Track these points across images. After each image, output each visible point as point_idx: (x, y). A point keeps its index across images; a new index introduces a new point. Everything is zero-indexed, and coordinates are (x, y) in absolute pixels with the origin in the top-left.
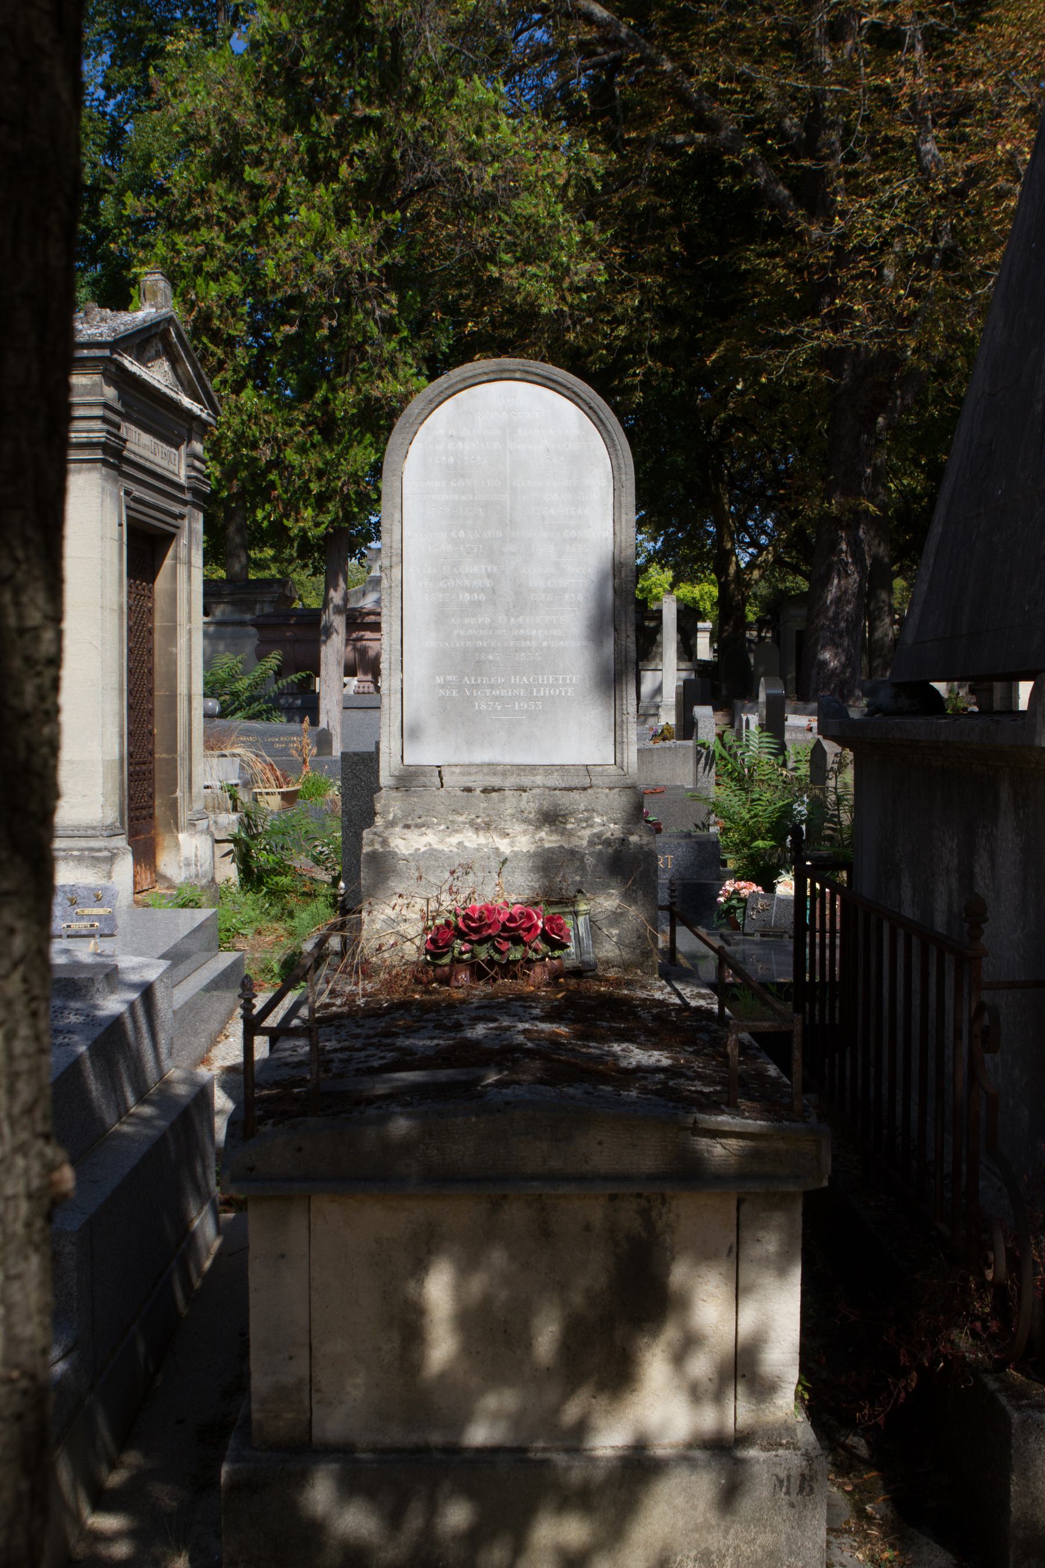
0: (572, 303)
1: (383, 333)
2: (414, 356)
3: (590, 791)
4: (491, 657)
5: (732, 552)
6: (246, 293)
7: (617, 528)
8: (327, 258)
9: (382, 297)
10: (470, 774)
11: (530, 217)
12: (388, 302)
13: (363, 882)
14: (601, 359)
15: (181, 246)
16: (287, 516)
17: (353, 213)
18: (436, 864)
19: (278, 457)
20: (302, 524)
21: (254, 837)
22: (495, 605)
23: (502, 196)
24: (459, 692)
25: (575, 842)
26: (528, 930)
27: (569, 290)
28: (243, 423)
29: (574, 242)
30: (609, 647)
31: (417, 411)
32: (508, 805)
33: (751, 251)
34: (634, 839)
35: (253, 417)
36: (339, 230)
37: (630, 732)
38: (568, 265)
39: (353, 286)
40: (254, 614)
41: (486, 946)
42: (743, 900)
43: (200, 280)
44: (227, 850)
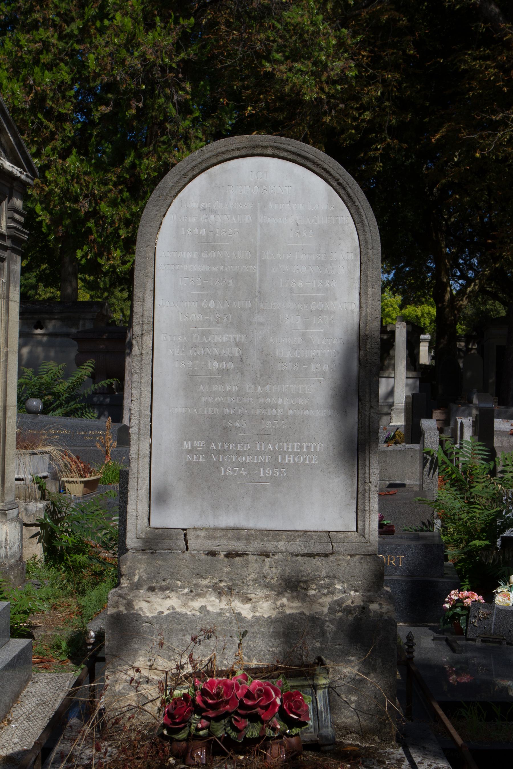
0: (329, 93)
1: (179, 114)
2: (204, 133)
3: (331, 558)
4: (237, 424)
5: (448, 284)
6: (74, 80)
7: (363, 301)
8: (136, 54)
9: (179, 85)
10: (214, 538)
11: (297, 24)
12: (183, 89)
13: (106, 643)
14: (351, 137)
15: (23, 42)
16: (101, 255)
17: (158, 19)
18: (179, 627)
19: (95, 208)
20: (112, 262)
21: (57, 521)
22: (242, 373)
23: (276, 9)
24: (206, 458)
25: (317, 608)
26: (266, 708)
27: (327, 83)
28: (67, 181)
29: (331, 45)
30: (353, 417)
31: (171, 184)
32: (251, 570)
33: (469, 55)
34: (374, 607)
35: (76, 178)
36: (147, 32)
37: (371, 501)
38: (326, 63)
39: (156, 76)
40: (78, 328)
41: (223, 722)
42: (467, 608)
43: (37, 69)
44: (34, 532)
